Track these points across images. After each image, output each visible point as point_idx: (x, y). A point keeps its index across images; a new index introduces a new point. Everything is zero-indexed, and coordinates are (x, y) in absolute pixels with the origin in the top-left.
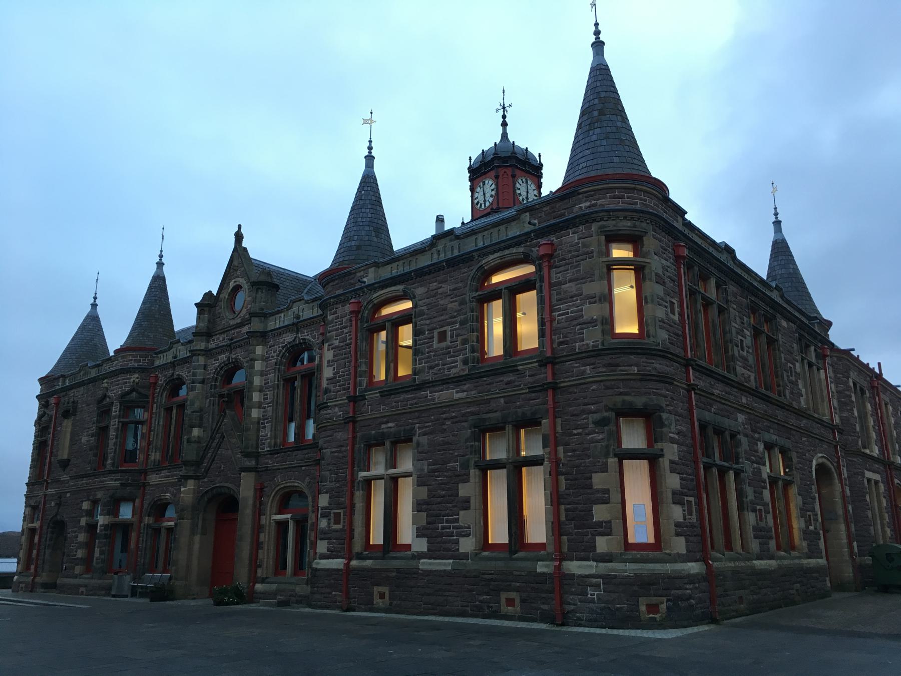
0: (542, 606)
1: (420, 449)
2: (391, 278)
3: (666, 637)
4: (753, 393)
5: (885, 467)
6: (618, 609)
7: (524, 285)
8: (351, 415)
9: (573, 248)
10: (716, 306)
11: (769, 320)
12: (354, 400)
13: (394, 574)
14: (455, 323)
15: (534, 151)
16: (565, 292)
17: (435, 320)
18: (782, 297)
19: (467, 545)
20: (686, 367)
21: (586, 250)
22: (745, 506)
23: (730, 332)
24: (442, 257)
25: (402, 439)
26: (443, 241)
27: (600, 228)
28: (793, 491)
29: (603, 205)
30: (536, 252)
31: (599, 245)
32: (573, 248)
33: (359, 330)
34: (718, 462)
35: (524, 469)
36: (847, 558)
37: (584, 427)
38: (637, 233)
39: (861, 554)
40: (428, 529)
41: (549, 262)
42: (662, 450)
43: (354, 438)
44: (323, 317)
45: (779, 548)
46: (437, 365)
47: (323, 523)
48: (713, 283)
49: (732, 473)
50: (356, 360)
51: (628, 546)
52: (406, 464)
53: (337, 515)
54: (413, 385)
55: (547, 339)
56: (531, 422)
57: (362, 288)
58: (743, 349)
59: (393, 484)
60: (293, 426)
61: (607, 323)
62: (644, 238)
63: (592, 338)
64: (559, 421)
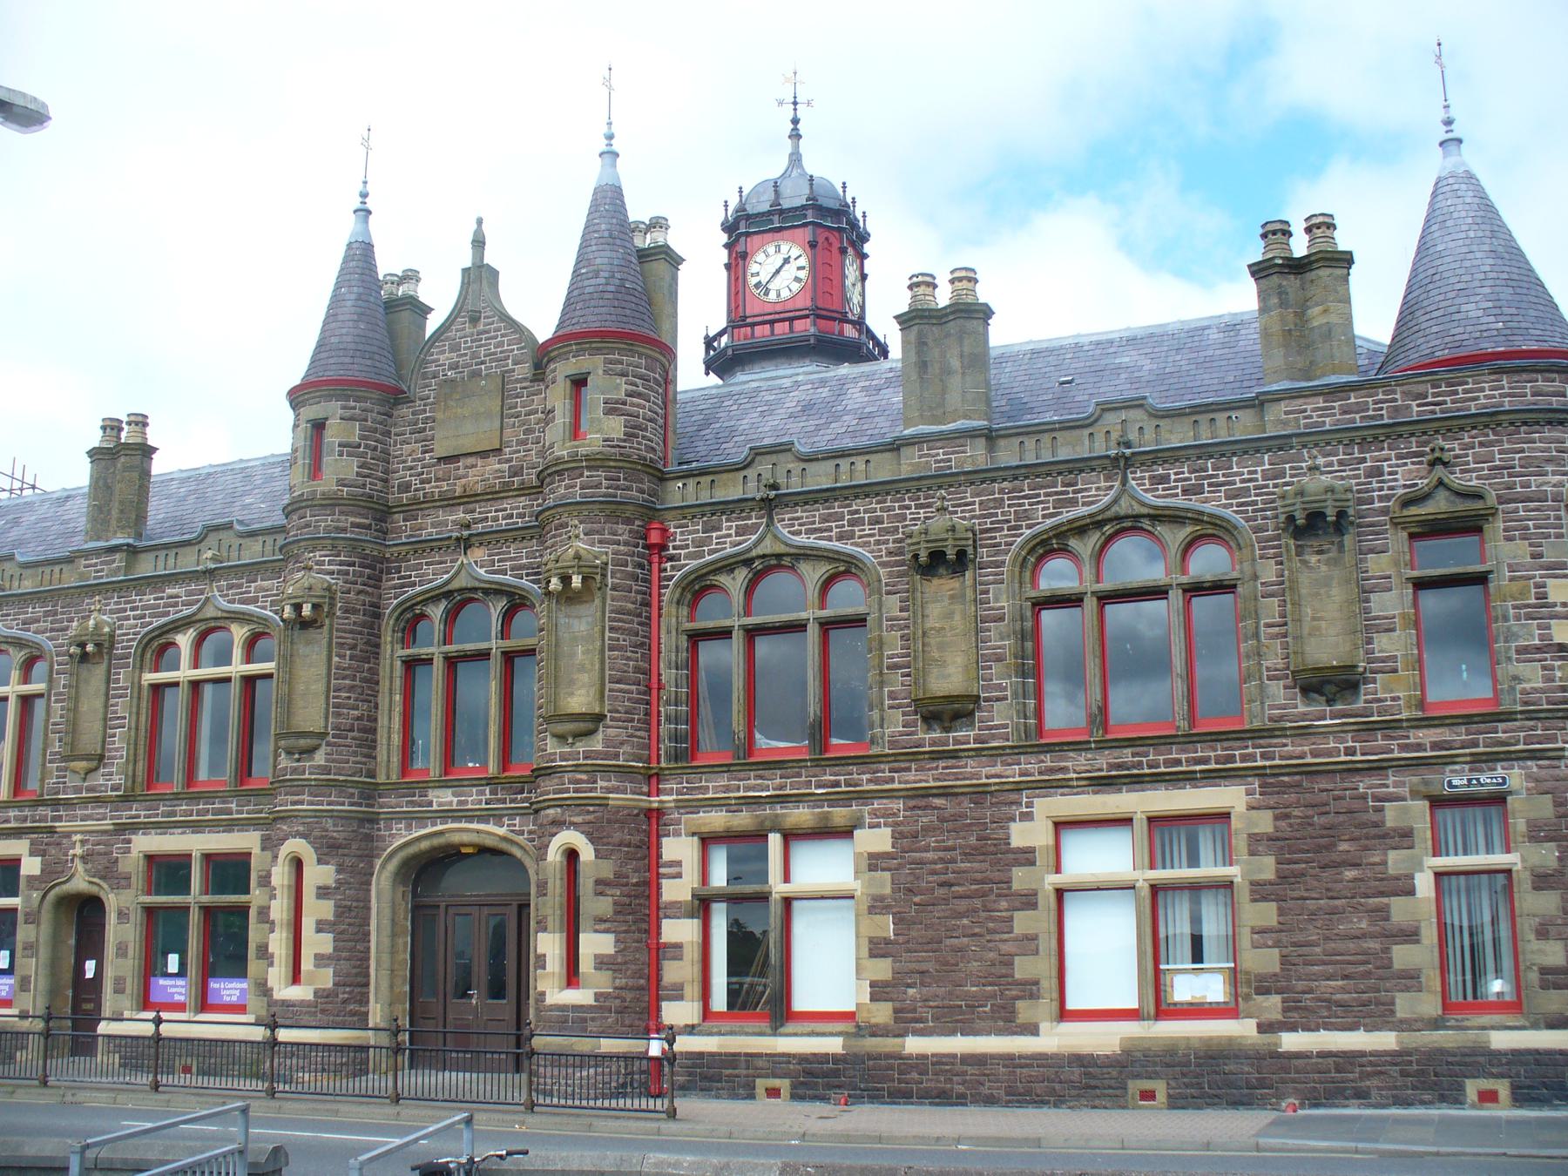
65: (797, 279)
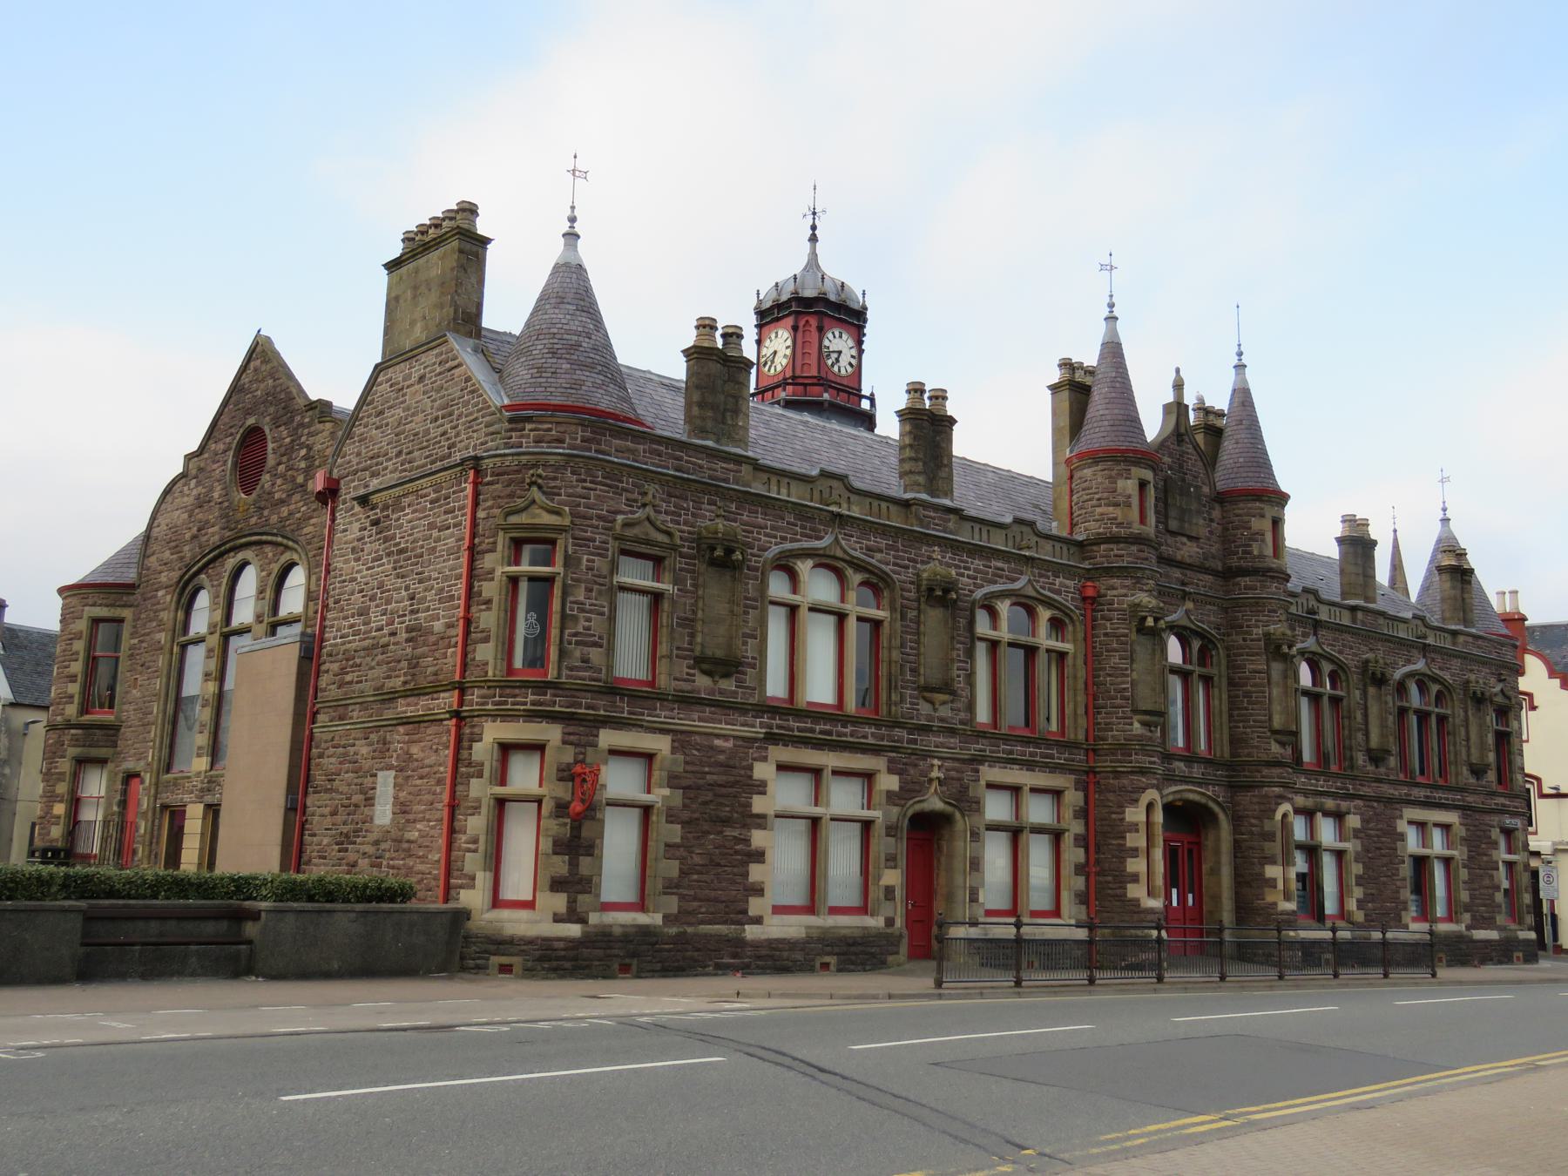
15: (856, 286)
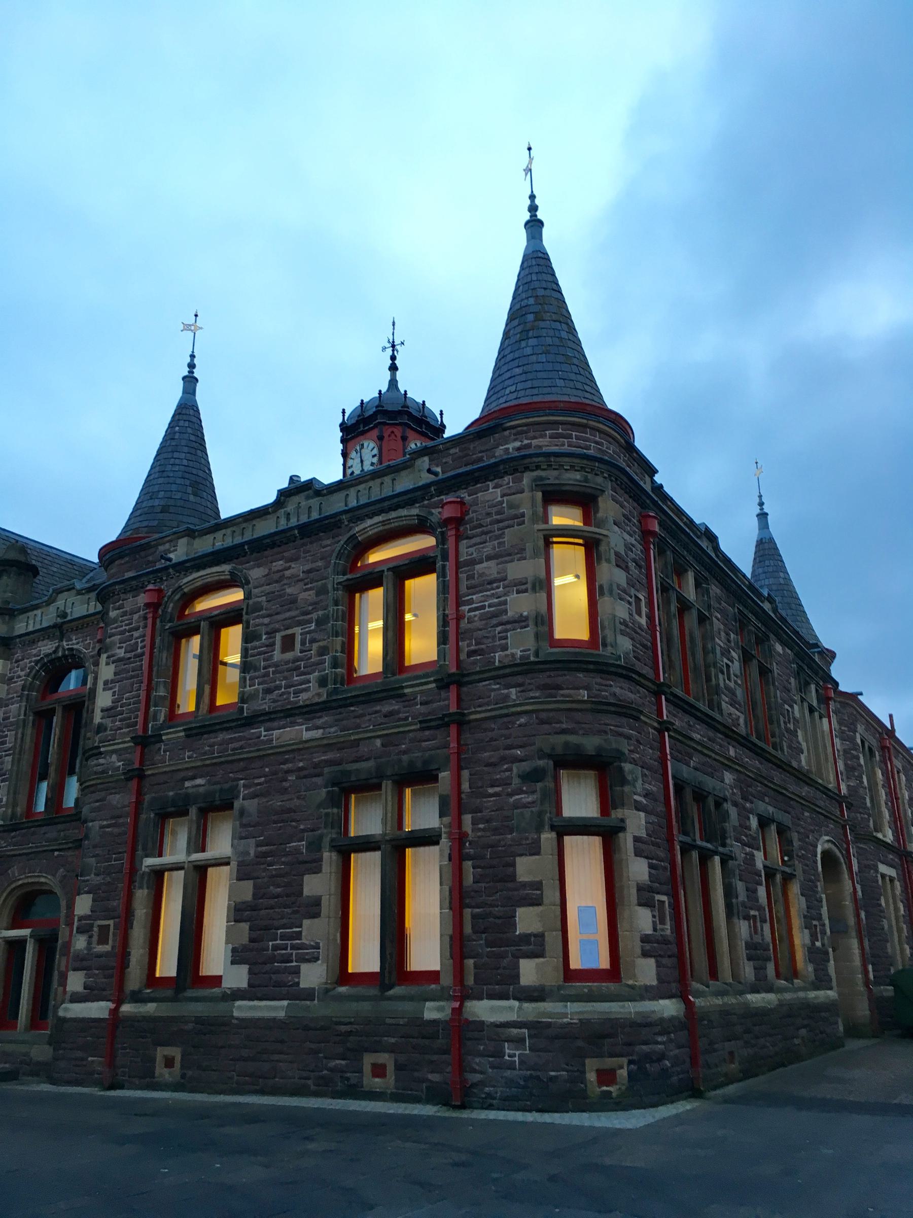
0: (430, 1076)
1: (245, 821)
2: (212, 553)
3: (629, 1126)
4: (743, 742)
5: (901, 859)
6: (552, 1079)
7: (418, 565)
8: (136, 766)
9: (494, 510)
10: (694, 613)
11: (761, 640)
12: (145, 742)
13: (190, 1026)
14: (309, 622)
15: (434, 407)
16: (481, 575)
17: (279, 617)
18: (775, 610)
19: (313, 975)
20: (657, 694)
21: (513, 512)
22: (735, 911)
23: (713, 651)
24: (294, 522)
25: (217, 805)
26: (295, 499)
27: (535, 480)
28: (795, 889)
29: (540, 447)
30: (437, 515)
31: (533, 504)
32: (494, 510)
33: (157, 633)
34: (699, 842)
35: (409, 851)
36: (861, 988)
37: (506, 783)
38: (589, 491)
39: (877, 982)
40: (252, 950)
41: (457, 530)
42: (623, 820)
43: (139, 803)
44: (103, 615)
45: (778, 975)
46: (278, 688)
47: (80, 943)
48: (690, 577)
49: (717, 859)
50: (150, 680)
51: (570, 975)
52: (222, 842)
53: (104, 929)
54: (241, 719)
55: (450, 647)
56: (420, 777)
57: (166, 568)
58: (729, 679)
59: (199, 875)
60: (44, 786)
61: (543, 624)
62: (600, 499)
63: (520, 645)
64: (465, 774)
65: (374, 456)
